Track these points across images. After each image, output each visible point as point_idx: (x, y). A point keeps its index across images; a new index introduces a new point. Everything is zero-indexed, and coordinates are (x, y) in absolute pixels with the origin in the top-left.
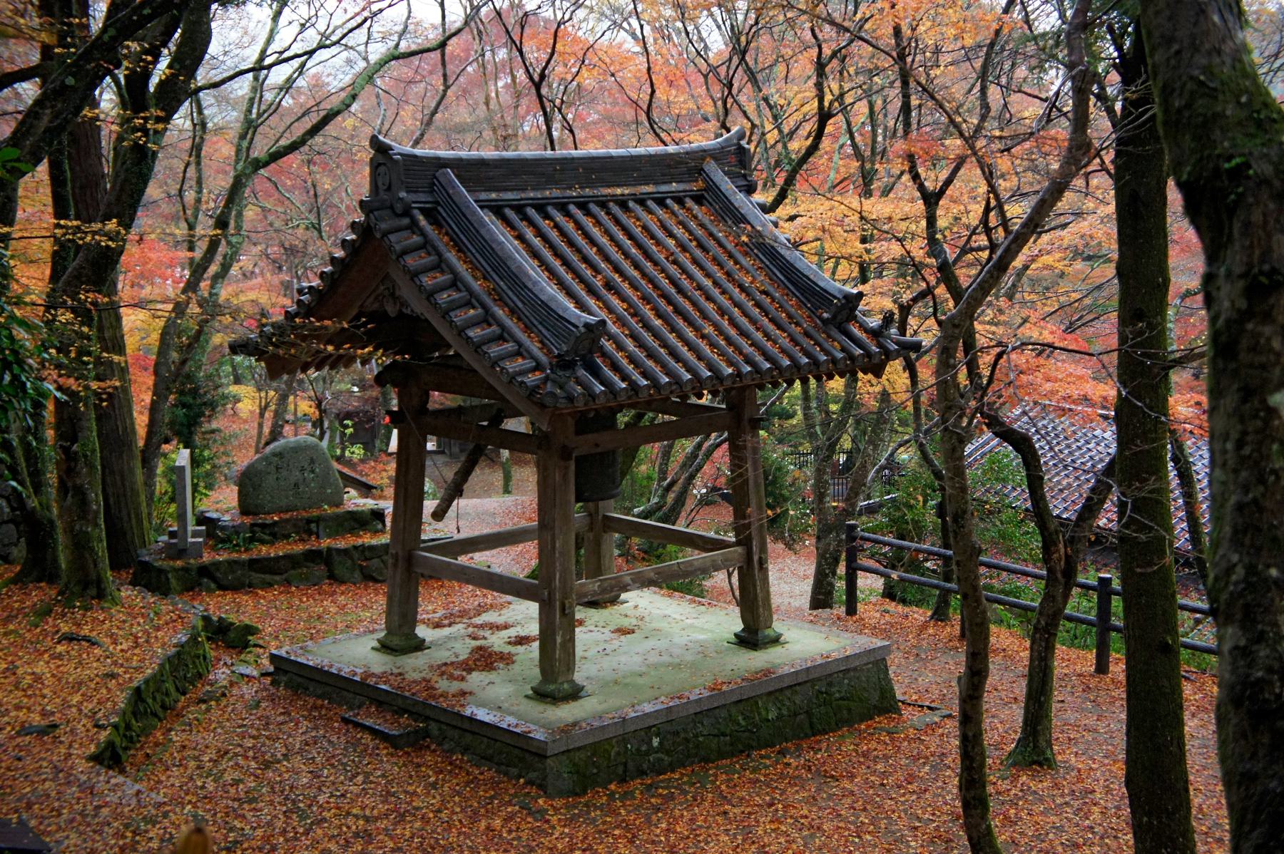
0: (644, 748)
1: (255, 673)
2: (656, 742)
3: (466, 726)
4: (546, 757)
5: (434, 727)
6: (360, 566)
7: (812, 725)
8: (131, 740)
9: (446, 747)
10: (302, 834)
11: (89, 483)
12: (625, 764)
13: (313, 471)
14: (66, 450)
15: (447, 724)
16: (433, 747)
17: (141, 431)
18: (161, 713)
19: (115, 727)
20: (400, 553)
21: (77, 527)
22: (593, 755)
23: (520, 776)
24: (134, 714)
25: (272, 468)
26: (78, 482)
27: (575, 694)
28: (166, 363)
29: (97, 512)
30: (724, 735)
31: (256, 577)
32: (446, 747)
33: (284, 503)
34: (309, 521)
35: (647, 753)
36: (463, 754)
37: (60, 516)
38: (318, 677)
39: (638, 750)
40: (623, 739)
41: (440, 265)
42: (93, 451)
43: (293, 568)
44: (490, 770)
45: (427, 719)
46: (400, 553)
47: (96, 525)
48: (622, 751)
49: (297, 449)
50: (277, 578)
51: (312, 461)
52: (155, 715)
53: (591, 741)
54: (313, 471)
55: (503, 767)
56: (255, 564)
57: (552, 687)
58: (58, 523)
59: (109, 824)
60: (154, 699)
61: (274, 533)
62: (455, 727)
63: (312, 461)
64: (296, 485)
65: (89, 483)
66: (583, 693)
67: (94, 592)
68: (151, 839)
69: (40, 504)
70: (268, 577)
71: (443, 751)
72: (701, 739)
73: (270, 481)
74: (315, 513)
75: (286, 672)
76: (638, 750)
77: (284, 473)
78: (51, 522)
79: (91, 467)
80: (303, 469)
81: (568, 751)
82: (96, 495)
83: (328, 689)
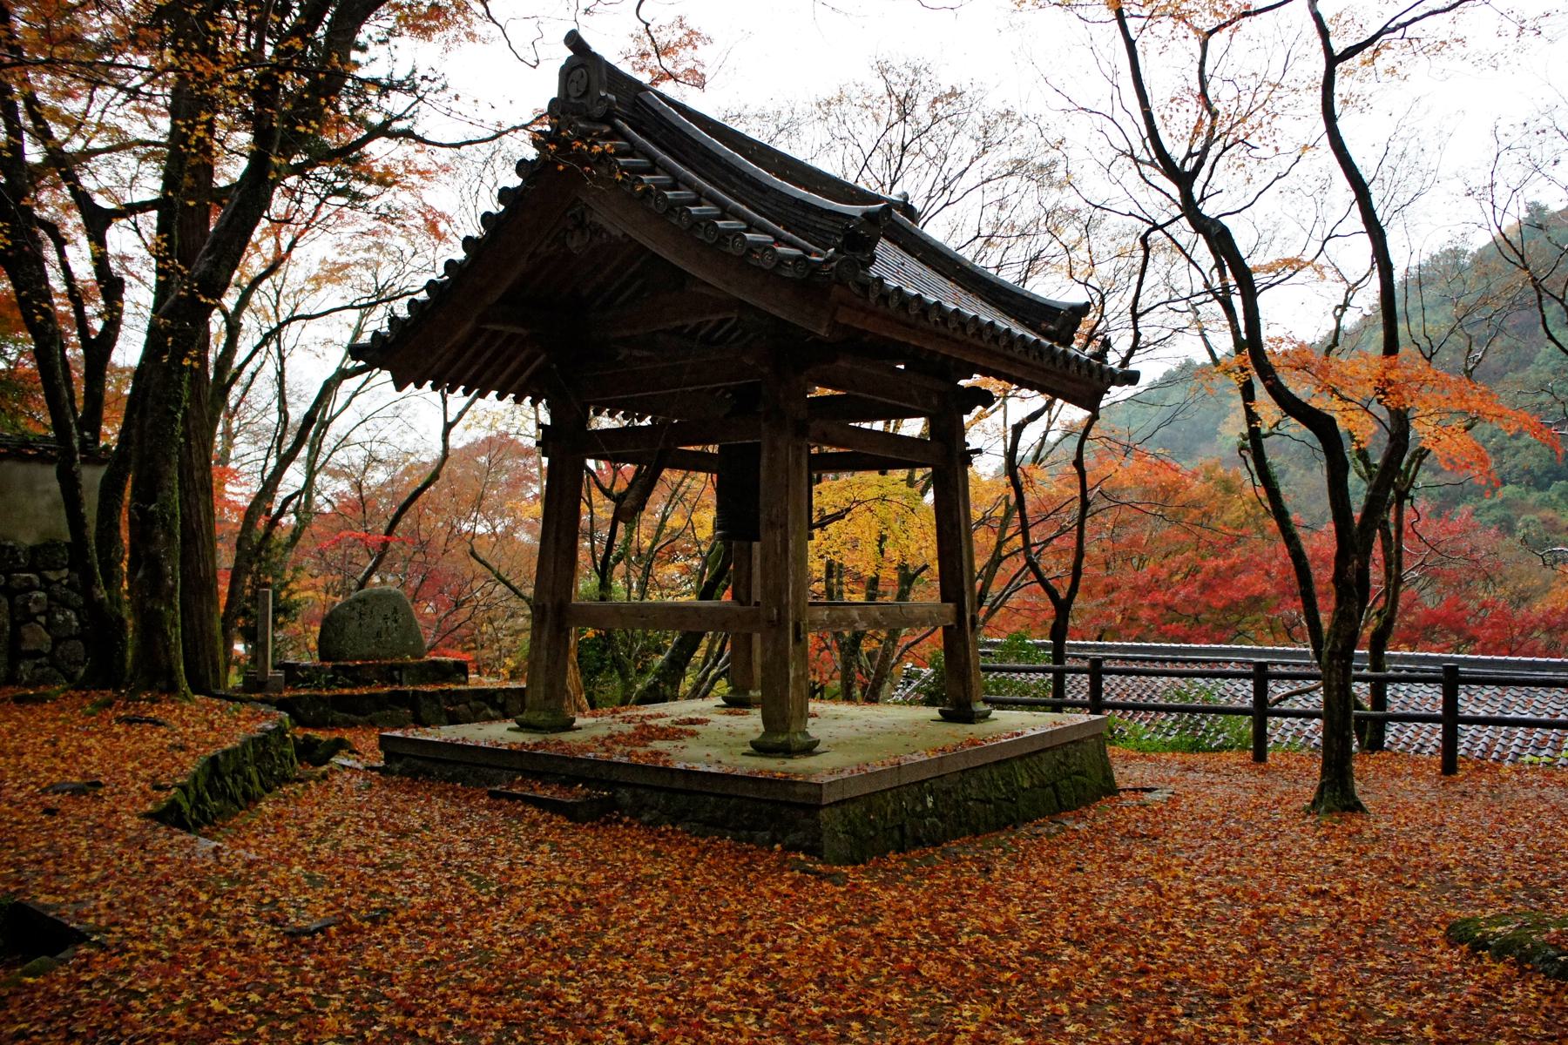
0: (919, 808)
1: (359, 766)
2: (930, 801)
3: (679, 784)
4: (819, 807)
5: (625, 795)
6: (447, 711)
7: (1059, 802)
8: (203, 814)
9: (646, 818)
10: (491, 903)
11: (166, 553)
12: (901, 828)
13: (396, 621)
14: (141, 512)
15: (645, 787)
16: (626, 819)
17: (223, 600)
18: (242, 802)
19: (183, 788)
20: (549, 605)
21: (149, 605)
22: (869, 810)
23: (774, 841)
24: (209, 787)
25: (355, 614)
26: (153, 549)
27: (809, 749)
28: (250, 539)
29: (173, 589)
30: (990, 802)
31: (338, 716)
32: (646, 818)
33: (366, 651)
34: (393, 667)
35: (922, 816)
36: (674, 825)
37: (132, 639)
38: (446, 756)
39: (913, 809)
40: (897, 791)
41: (654, 166)
42: (173, 516)
43: (379, 710)
44: (722, 837)
45: (613, 785)
46: (549, 605)
47: (171, 605)
48: (898, 808)
49: (382, 597)
50: (361, 719)
51: (395, 611)
52: (235, 801)
53: (867, 790)
54: (396, 621)
55: (744, 833)
56: (339, 702)
57: (781, 739)
58: (130, 622)
59: (169, 884)
60: (235, 781)
61: (356, 677)
62: (659, 789)
63: (395, 611)
64: (379, 634)
65: (166, 553)
66: (817, 749)
67: (163, 685)
68: (242, 901)
69: (110, 597)
70: (352, 717)
71: (642, 823)
72: (970, 803)
73: (352, 627)
74: (398, 661)
75: (399, 757)
76: (913, 809)
77: (367, 620)
78: (122, 621)
79: (171, 534)
80: (386, 618)
81: (843, 801)
82: (173, 569)
83: (460, 769)
